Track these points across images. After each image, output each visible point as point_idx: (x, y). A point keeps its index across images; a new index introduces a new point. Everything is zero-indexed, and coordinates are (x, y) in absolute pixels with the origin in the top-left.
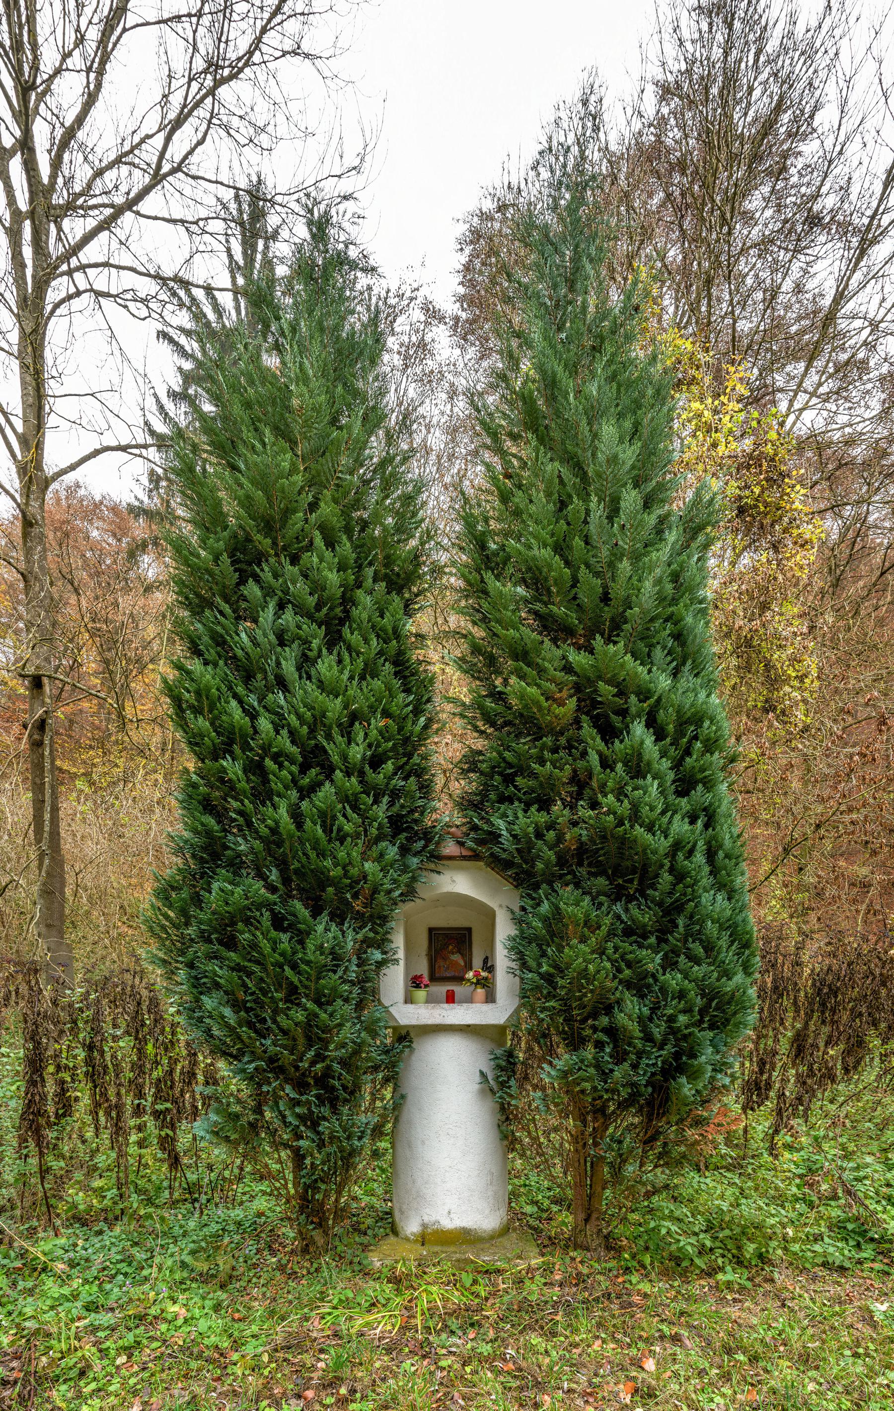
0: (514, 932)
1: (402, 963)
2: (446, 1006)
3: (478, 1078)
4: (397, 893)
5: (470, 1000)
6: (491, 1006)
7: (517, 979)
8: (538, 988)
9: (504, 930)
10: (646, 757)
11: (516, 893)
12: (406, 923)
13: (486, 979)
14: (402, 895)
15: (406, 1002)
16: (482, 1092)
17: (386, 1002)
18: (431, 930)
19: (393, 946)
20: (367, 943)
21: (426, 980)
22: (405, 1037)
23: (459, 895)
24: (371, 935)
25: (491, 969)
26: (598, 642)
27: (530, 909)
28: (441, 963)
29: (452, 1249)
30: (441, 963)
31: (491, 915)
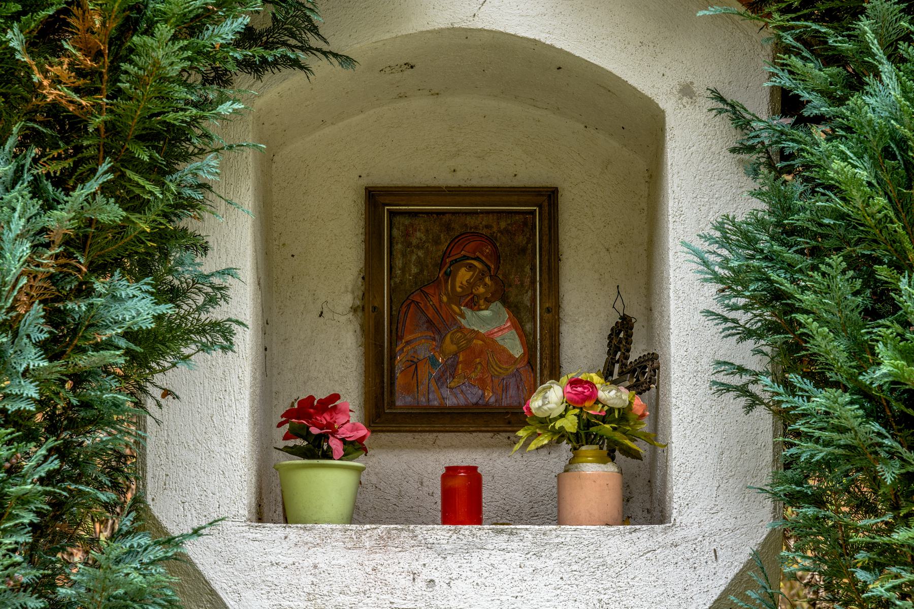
0: (744, 203)
1: (246, 340)
2: (442, 533)
4: (228, 29)
5: (551, 510)
6: (644, 536)
7: (763, 418)
8: (857, 455)
9: (703, 194)
11: (756, 37)
12: (267, 166)
13: (621, 417)
14: (248, 36)
15: (260, 516)
17: (171, 514)
18: (375, 199)
19: (208, 264)
20: (92, 254)
21: (352, 417)
24: (111, 212)
25: (644, 374)
26: (71, 193)
27: (817, 105)
28: (418, 345)
30: (418, 345)
31: (641, 132)
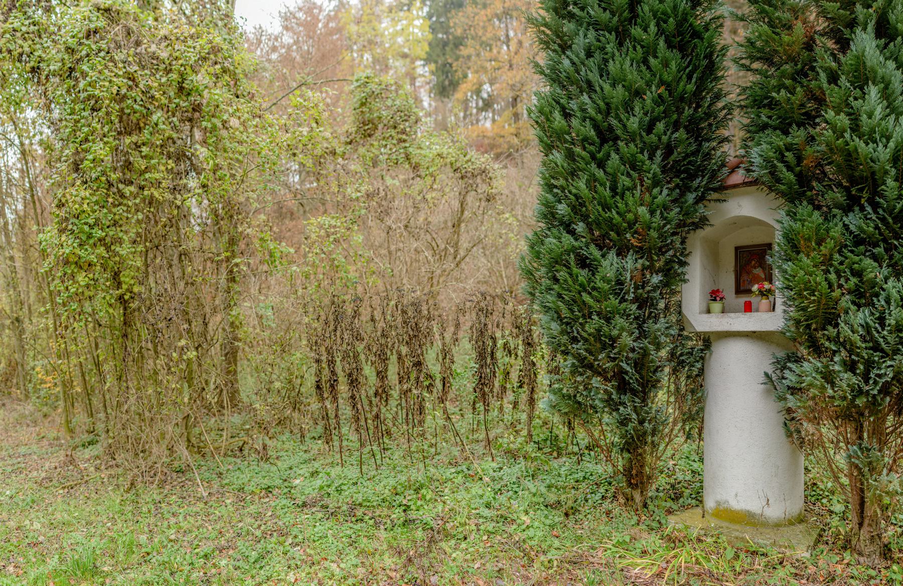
3: (762, 379)
6: (771, 314)
10: (869, 64)
16: (768, 391)
18: (737, 249)
22: (708, 341)
23: (751, 217)
29: (737, 527)
30: (745, 277)
